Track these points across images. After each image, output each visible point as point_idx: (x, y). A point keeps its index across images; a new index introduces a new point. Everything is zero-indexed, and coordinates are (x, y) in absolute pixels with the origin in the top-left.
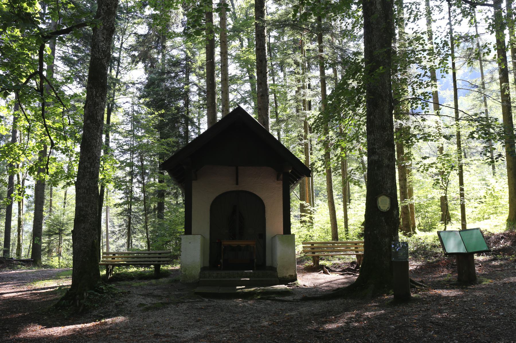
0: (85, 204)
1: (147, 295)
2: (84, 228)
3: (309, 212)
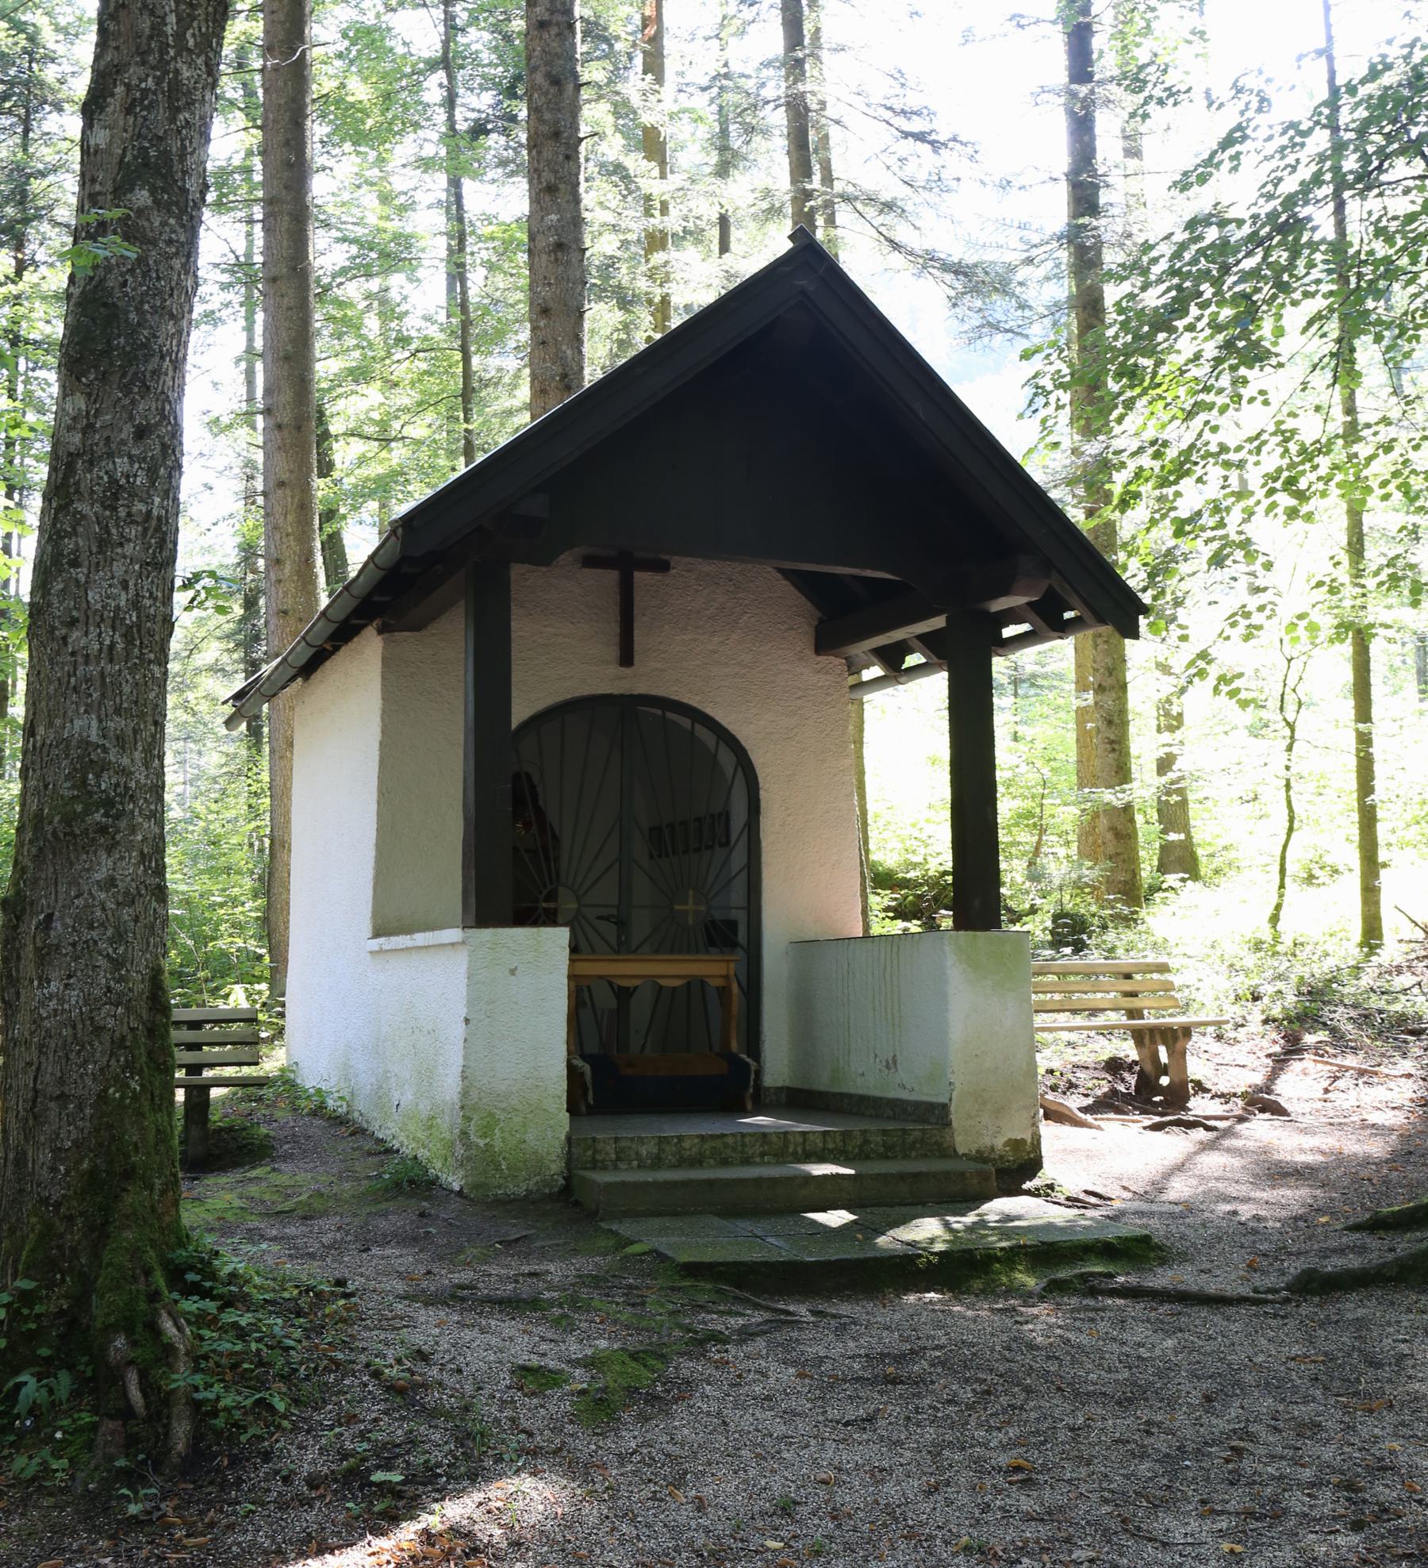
0: (115, 724)
1: (453, 1296)
2: (111, 882)
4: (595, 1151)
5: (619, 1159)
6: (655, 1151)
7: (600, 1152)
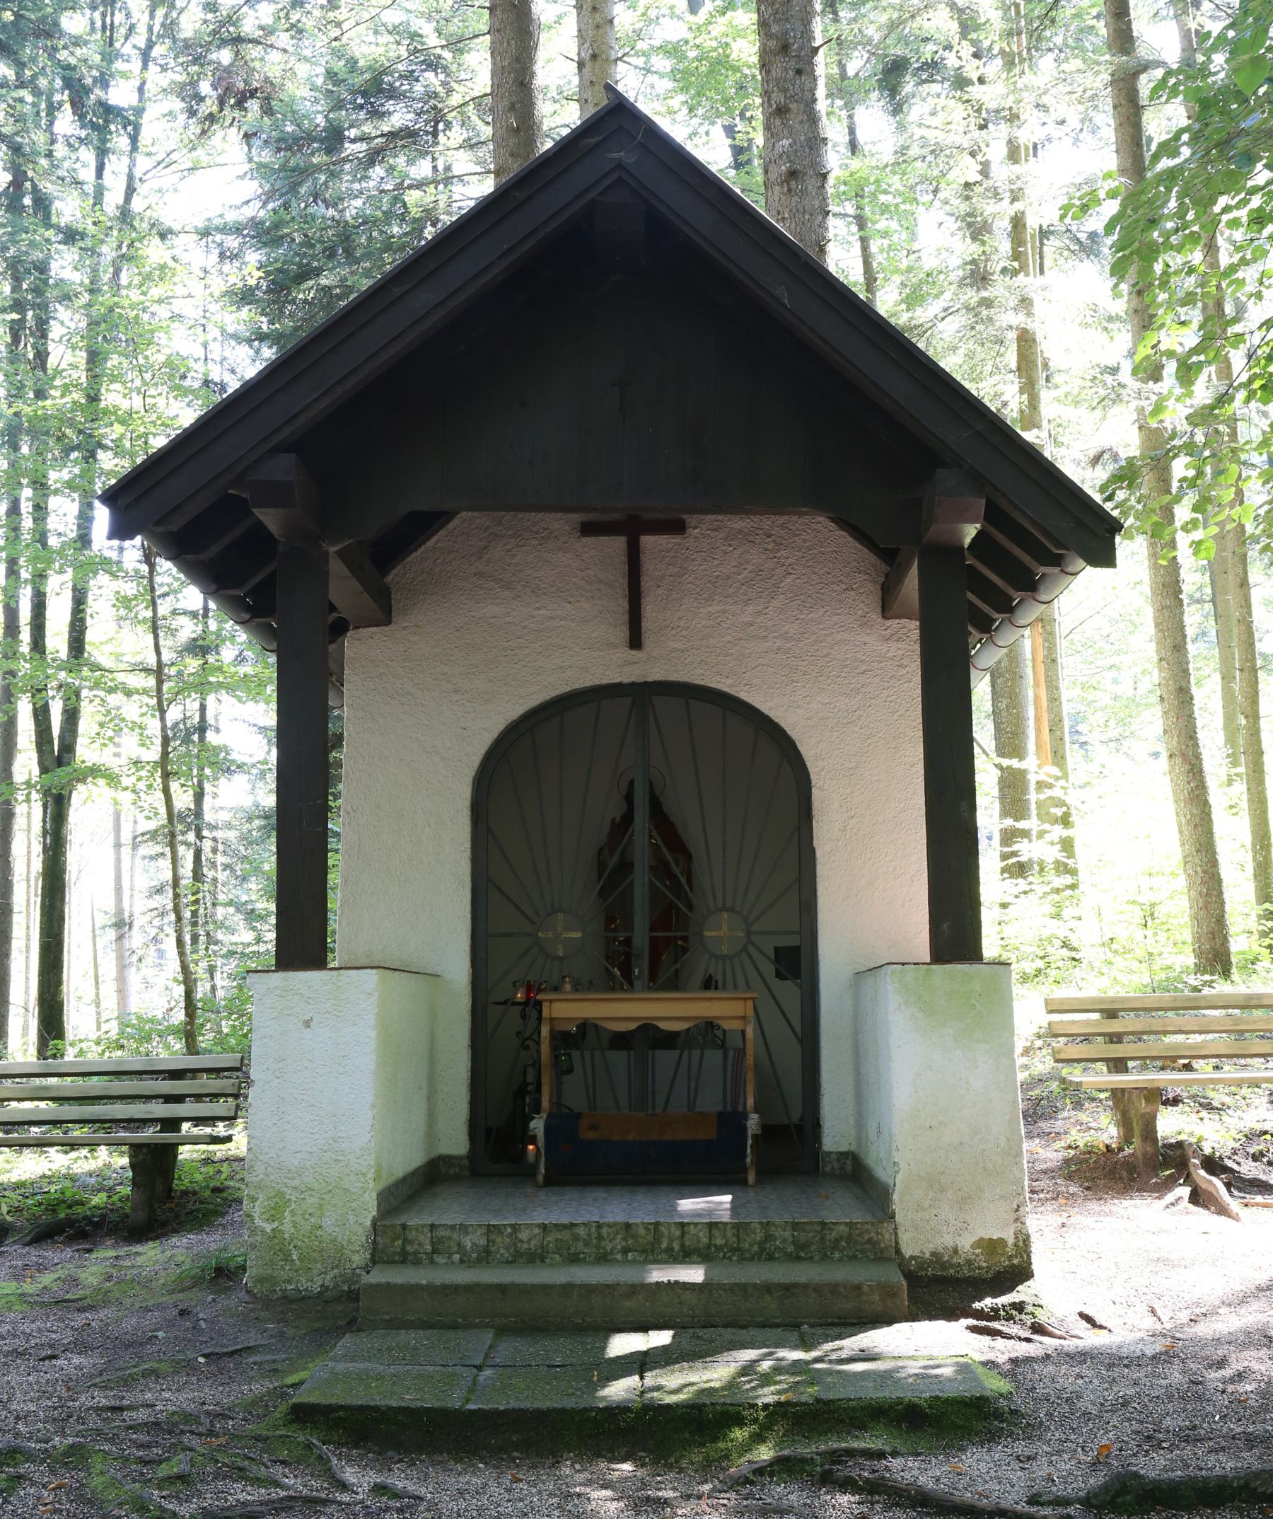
3: (1059, 812)
4: (406, 1241)
5: (435, 1251)
6: (483, 1242)
7: (411, 1242)
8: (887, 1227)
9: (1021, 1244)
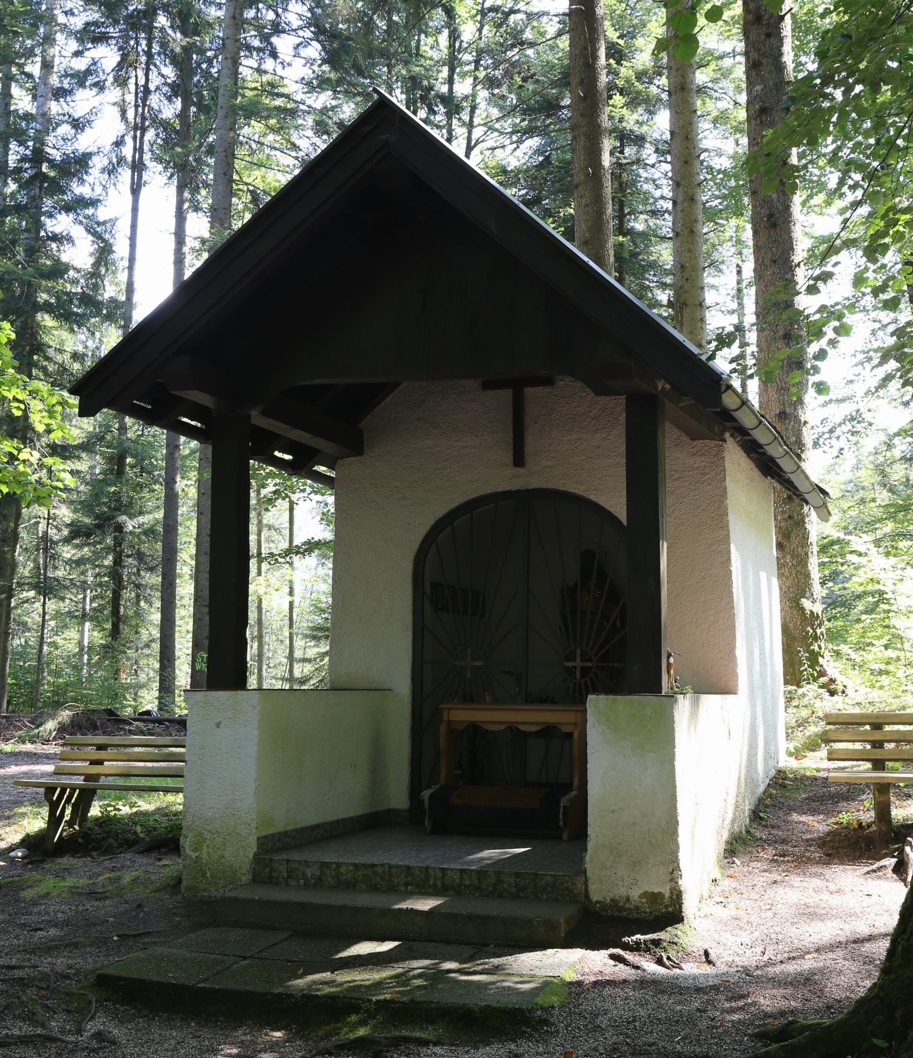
6: (318, 873)
8: (580, 880)
9: (675, 897)
